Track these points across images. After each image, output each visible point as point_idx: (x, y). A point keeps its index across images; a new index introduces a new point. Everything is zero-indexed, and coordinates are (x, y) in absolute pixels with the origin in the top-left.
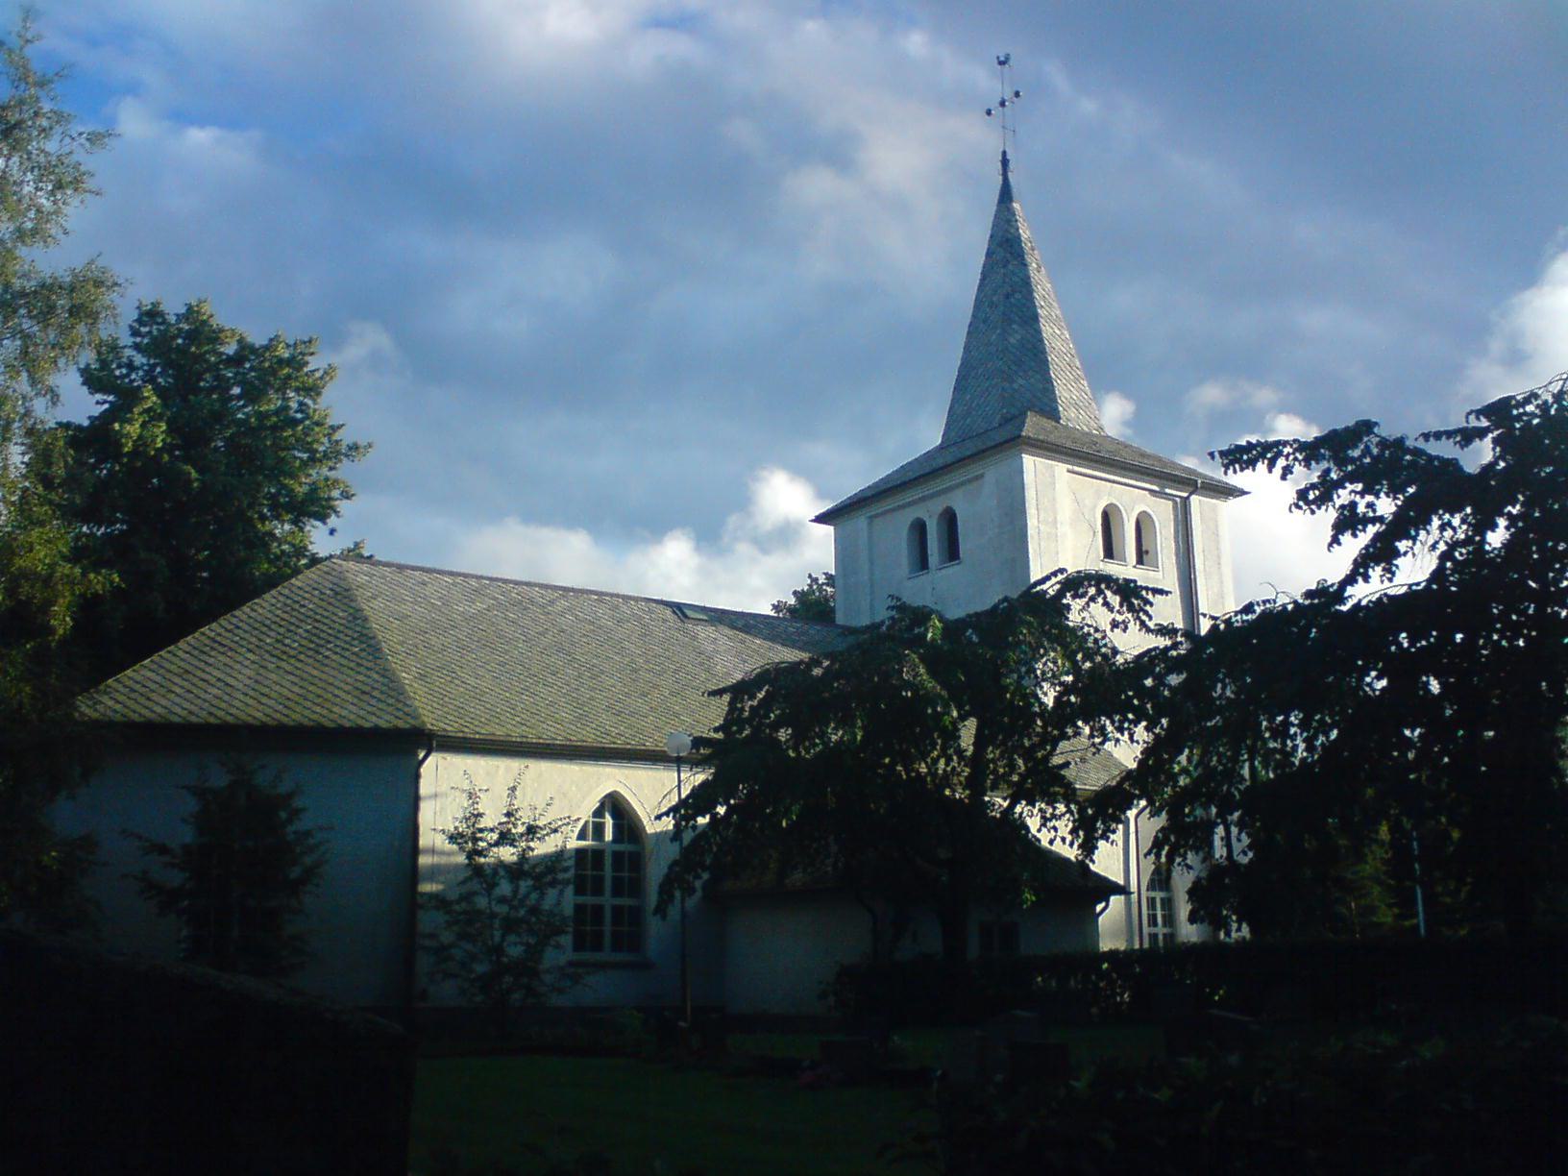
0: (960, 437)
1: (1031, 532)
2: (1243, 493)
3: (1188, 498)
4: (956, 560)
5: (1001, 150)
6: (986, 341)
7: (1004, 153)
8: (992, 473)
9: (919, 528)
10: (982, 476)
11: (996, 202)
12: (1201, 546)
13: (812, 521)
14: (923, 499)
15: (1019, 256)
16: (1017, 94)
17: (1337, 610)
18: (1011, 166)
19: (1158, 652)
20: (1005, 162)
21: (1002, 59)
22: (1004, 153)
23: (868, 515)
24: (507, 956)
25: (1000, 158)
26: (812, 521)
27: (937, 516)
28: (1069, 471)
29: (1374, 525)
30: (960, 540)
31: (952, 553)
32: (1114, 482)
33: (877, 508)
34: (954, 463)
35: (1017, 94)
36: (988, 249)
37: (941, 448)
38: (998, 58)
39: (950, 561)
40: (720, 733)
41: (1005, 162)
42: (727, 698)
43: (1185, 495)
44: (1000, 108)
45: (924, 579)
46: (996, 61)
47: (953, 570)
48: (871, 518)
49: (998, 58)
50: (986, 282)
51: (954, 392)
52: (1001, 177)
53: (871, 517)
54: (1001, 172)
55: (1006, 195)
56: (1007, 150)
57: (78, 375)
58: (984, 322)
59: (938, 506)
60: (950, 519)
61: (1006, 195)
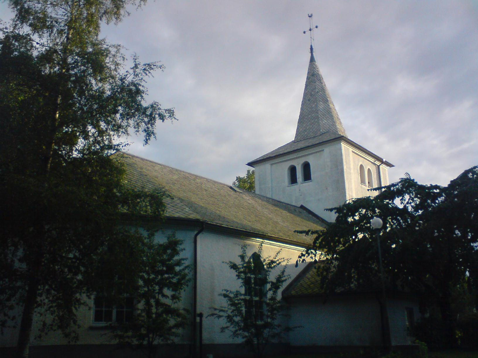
0: (302, 139)
1: (345, 171)
2: (393, 166)
3: (379, 166)
4: (310, 180)
5: (310, 45)
6: (311, 107)
7: (311, 46)
8: (327, 150)
9: (293, 170)
10: (323, 150)
11: (309, 61)
12: (347, 186)
13: (247, 165)
14: (297, 158)
15: (320, 80)
16: (304, 32)
17: (473, 218)
18: (314, 50)
19: (460, 229)
20: (312, 49)
21: (310, 15)
22: (311, 46)
23: (271, 163)
24: (240, 317)
25: (310, 47)
26: (247, 165)
27: (301, 164)
28: (353, 152)
29: (384, 188)
30: (311, 173)
31: (307, 176)
32: (364, 158)
33: (276, 161)
34: (312, 146)
35: (304, 32)
36: (307, 77)
37: (294, 142)
38: (308, 15)
39: (305, 181)
40: (343, 242)
41: (312, 49)
42: (315, 236)
43: (379, 165)
44: (309, 31)
45: (295, 186)
46: (308, 16)
47: (308, 184)
48: (272, 164)
49: (308, 15)
50: (308, 87)
51: (298, 123)
52: (310, 54)
53: (271, 164)
54: (310, 52)
55: (312, 60)
56: (312, 45)
57: (122, 14)
58: (309, 100)
59: (302, 161)
60: (306, 167)
61: (312, 60)
